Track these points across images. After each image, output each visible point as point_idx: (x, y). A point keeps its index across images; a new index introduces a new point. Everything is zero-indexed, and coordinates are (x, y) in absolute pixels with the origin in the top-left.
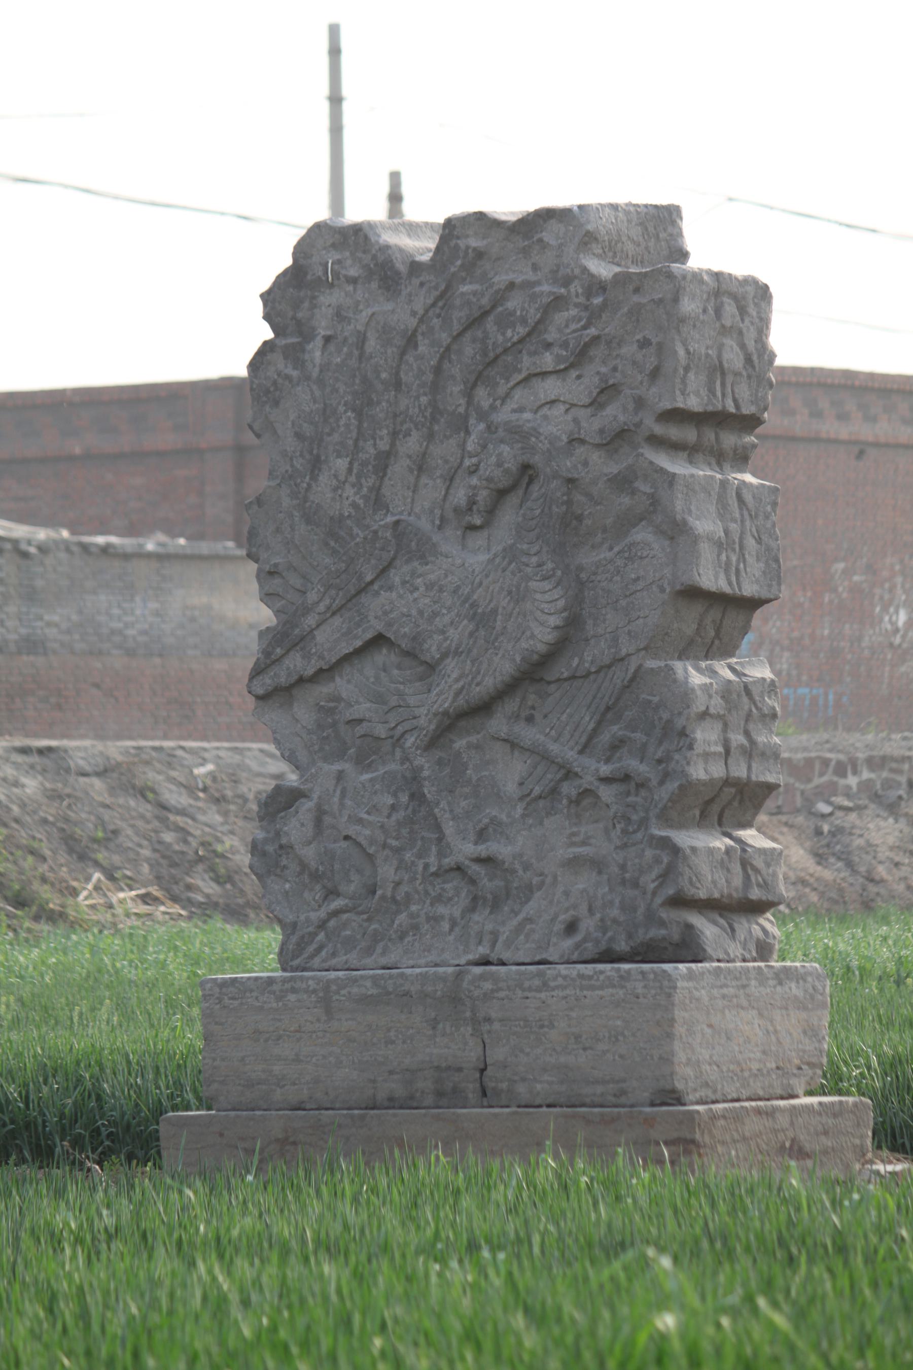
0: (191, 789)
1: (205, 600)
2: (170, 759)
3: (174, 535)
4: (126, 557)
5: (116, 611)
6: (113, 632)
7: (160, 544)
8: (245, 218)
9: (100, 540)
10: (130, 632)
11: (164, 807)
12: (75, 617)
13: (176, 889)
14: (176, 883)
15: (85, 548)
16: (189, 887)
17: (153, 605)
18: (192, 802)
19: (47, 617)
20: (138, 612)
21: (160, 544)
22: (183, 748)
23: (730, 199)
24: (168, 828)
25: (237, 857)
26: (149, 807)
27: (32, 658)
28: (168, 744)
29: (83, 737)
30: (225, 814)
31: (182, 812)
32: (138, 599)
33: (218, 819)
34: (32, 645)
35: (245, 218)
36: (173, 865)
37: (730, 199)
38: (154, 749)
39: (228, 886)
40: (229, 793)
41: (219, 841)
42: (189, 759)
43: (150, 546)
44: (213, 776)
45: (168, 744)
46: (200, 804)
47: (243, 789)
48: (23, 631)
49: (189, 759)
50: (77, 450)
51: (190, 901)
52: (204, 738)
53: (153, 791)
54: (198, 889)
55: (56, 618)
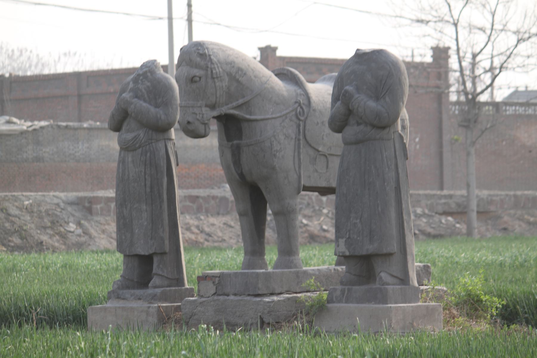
0: (21, 209)
1: (107, 143)
2: (16, 199)
3: (96, 121)
4: (75, 129)
5: (71, 147)
6: (70, 154)
7: (89, 124)
8: (127, 14)
9: (64, 124)
10: (77, 154)
11: (9, 215)
12: (55, 150)
13: (5, 242)
14: (5, 239)
15: (59, 127)
16: (10, 241)
17: (86, 145)
18: (20, 213)
19: (44, 150)
20: (80, 147)
21: (89, 124)
22: (23, 195)
23: (315, 3)
24: (8, 221)
25: (32, 231)
26: (3, 215)
27: (38, 164)
28: (16, 194)
29: (17, 192)
30: (32, 217)
31: (16, 216)
32: (80, 143)
33: (29, 218)
34: (38, 159)
35: (127, 14)
36: (6, 233)
37: (315, 3)
38: (12, 196)
39: (25, 240)
40: (35, 210)
41: (26, 225)
42: (23, 198)
43: (85, 125)
44: (31, 205)
45: (16, 194)
46: (23, 214)
47: (41, 208)
48: (35, 155)
49: (23, 198)
50: (112, 90)
51: (9, 246)
52: (31, 191)
53: (6, 210)
54: (12, 241)
55: (48, 150)
